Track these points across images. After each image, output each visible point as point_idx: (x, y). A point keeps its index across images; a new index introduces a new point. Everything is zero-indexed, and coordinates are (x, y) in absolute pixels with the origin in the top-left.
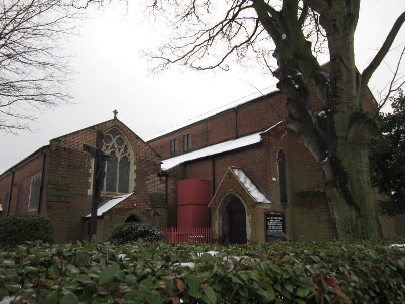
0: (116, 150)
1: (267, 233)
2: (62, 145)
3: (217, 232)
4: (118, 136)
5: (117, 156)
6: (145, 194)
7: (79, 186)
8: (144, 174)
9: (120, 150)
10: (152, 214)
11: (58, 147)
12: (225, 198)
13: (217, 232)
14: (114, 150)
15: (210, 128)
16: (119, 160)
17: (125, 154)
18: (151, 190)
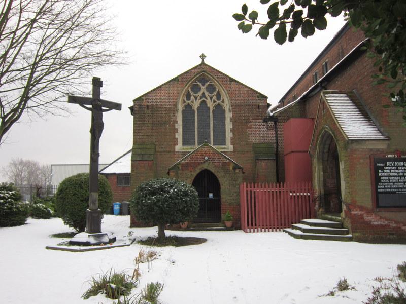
0: (206, 98)
1: (377, 188)
2: (145, 103)
3: (317, 188)
4: (208, 83)
5: (208, 106)
6: (246, 144)
7: (166, 143)
8: (244, 121)
9: (211, 98)
10: (231, 168)
11: (140, 107)
12: (322, 141)
13: (317, 188)
14: (204, 99)
15: (345, 46)
16: (211, 110)
17: (188, 102)
18: (254, 140)
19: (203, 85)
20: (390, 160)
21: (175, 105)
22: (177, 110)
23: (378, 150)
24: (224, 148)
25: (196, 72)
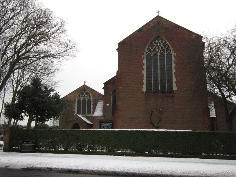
2: (65, 99)
9: (87, 97)
10: (83, 122)
19: (85, 92)
20: (104, 122)
21: (75, 100)
22: (75, 102)
23: (102, 119)
24: (90, 115)
25: (82, 88)
